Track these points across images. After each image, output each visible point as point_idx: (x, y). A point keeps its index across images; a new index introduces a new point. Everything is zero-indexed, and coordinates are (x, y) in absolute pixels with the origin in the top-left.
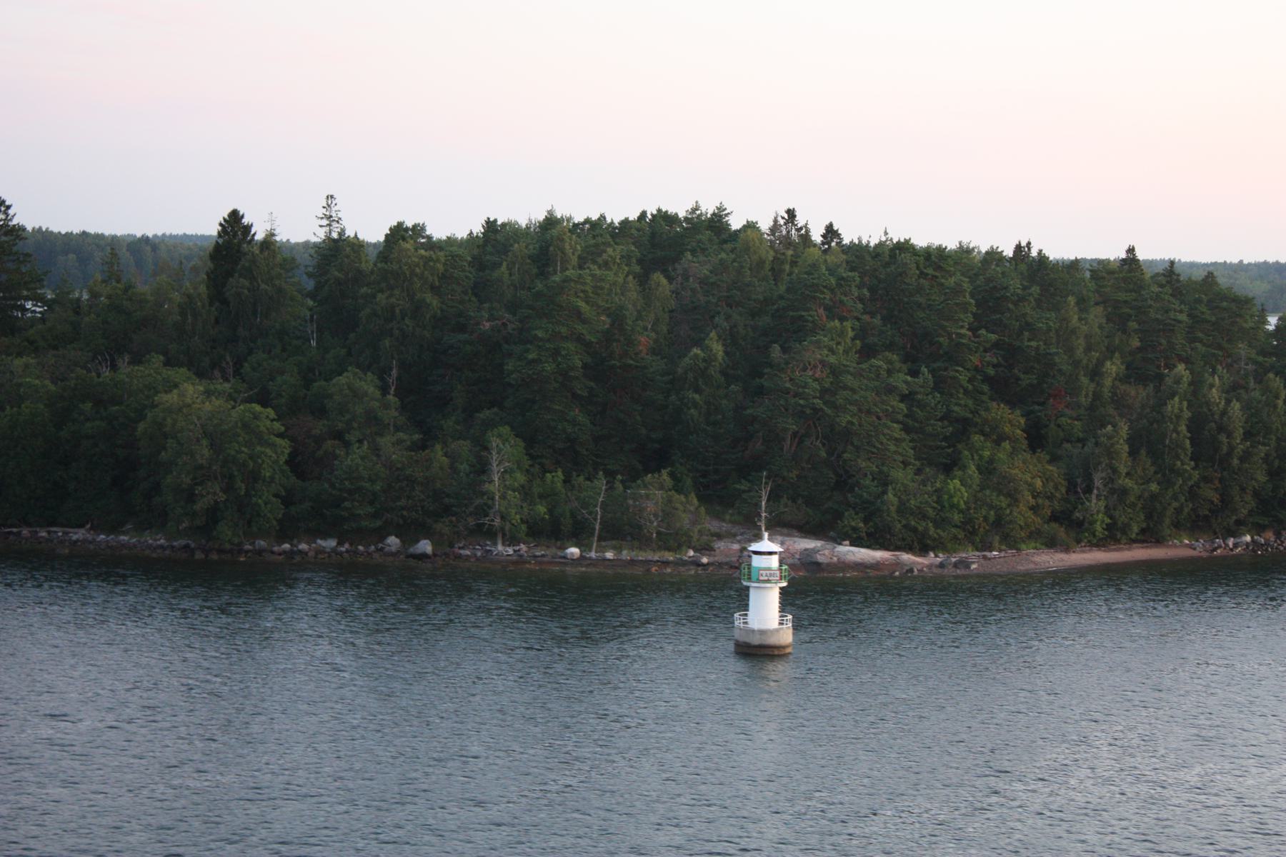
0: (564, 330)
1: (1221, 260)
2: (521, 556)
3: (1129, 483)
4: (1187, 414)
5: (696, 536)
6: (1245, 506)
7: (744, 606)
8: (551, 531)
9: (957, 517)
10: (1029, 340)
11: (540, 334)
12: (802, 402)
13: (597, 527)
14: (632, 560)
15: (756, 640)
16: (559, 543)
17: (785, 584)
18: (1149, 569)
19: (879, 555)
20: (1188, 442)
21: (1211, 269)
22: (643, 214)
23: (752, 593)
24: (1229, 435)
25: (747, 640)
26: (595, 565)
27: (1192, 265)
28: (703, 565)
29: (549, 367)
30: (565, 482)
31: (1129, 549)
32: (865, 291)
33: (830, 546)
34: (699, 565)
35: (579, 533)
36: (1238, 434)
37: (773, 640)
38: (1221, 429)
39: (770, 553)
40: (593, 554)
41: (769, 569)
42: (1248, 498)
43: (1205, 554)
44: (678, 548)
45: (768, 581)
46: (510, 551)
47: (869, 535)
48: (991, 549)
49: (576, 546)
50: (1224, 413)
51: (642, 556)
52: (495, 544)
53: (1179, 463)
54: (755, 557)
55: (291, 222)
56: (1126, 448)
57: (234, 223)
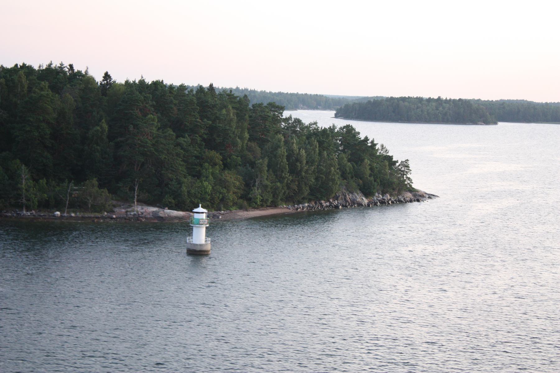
0: (41, 118)
3: (268, 183)
4: (286, 154)
6: (306, 191)
7: (191, 234)
8: (45, 205)
9: (209, 197)
10: (219, 123)
11: (31, 119)
12: (146, 149)
13: (67, 203)
14: (82, 217)
15: (198, 249)
16: (49, 210)
17: (208, 225)
21: (247, 94)
22: (16, 65)
23: (194, 229)
25: (194, 248)
28: (114, 218)
34: (112, 218)
35: (59, 205)
37: (205, 248)
39: (203, 213)
40: (65, 214)
41: (203, 219)
43: (294, 211)
44: (100, 211)
45: (202, 224)
46: (29, 214)
47: (176, 205)
48: (220, 210)
49: (58, 211)
51: (87, 215)
53: (284, 174)
54: (195, 214)
55: (548, 102)
57: (211, 85)
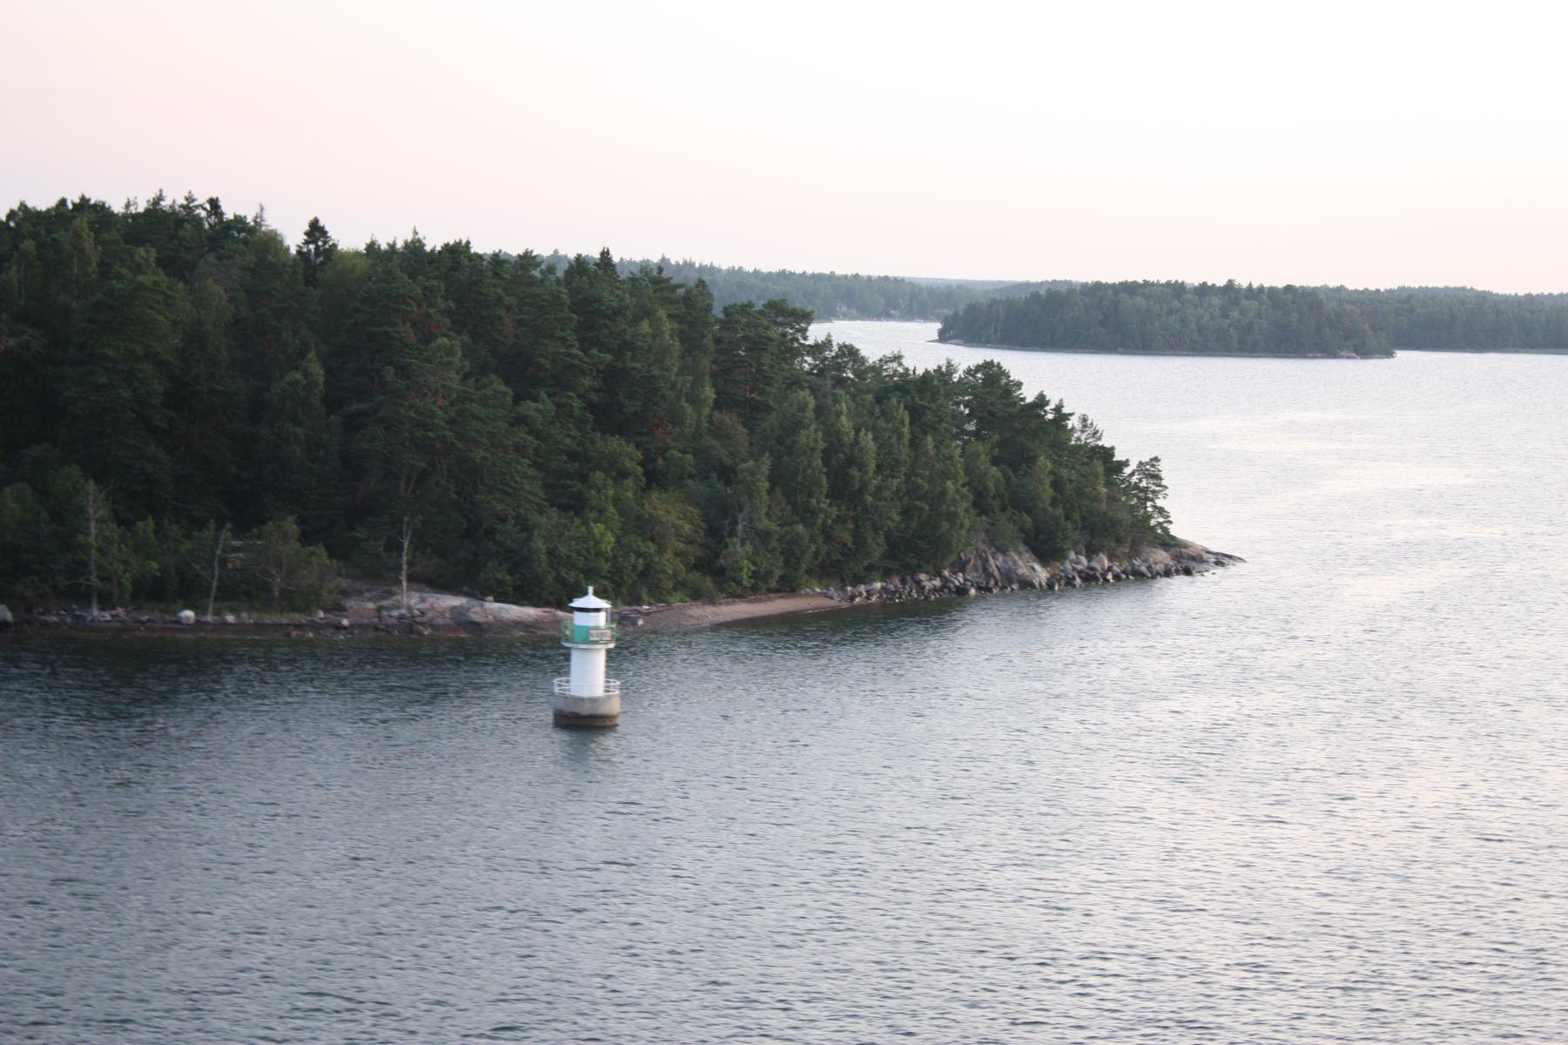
0: (139, 349)
1: (1333, 284)
2: (122, 622)
4: (822, 445)
5: (324, 593)
6: (877, 549)
8: (153, 592)
9: (606, 567)
11: (111, 353)
13: (215, 585)
15: (585, 710)
17: (612, 646)
18: (717, 627)
19: (530, 612)
20: (824, 478)
22: (63, 202)
23: (575, 656)
24: (862, 467)
25: (576, 710)
26: (213, 631)
27: (736, 274)
28: (345, 628)
29: (126, 394)
30: (156, 532)
31: (728, 604)
32: (452, 303)
33: (474, 602)
34: (339, 628)
35: (190, 592)
36: (872, 466)
38: (851, 461)
39: (598, 610)
40: (209, 618)
41: (597, 628)
42: (881, 539)
43: (845, 605)
44: (306, 609)
45: (596, 642)
46: (108, 617)
47: (516, 589)
48: (639, 602)
50: (856, 442)
51: (268, 619)
52: (89, 607)
54: (577, 615)
56: (767, 485)
